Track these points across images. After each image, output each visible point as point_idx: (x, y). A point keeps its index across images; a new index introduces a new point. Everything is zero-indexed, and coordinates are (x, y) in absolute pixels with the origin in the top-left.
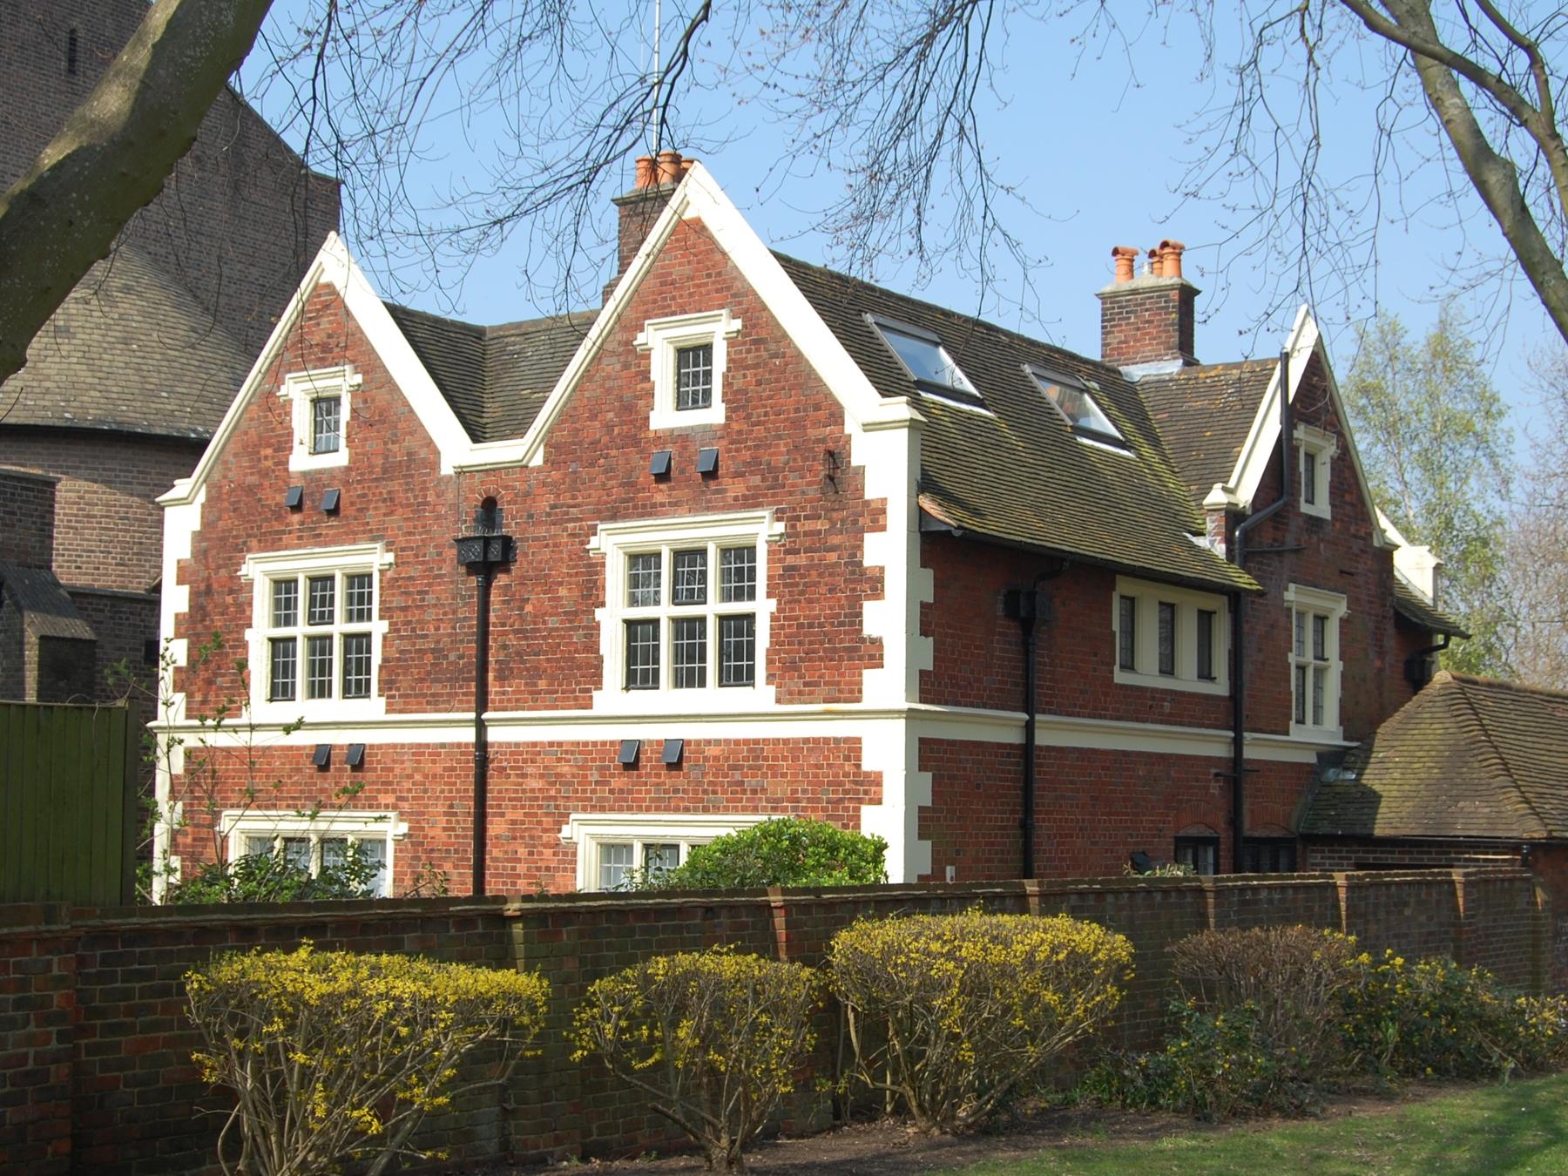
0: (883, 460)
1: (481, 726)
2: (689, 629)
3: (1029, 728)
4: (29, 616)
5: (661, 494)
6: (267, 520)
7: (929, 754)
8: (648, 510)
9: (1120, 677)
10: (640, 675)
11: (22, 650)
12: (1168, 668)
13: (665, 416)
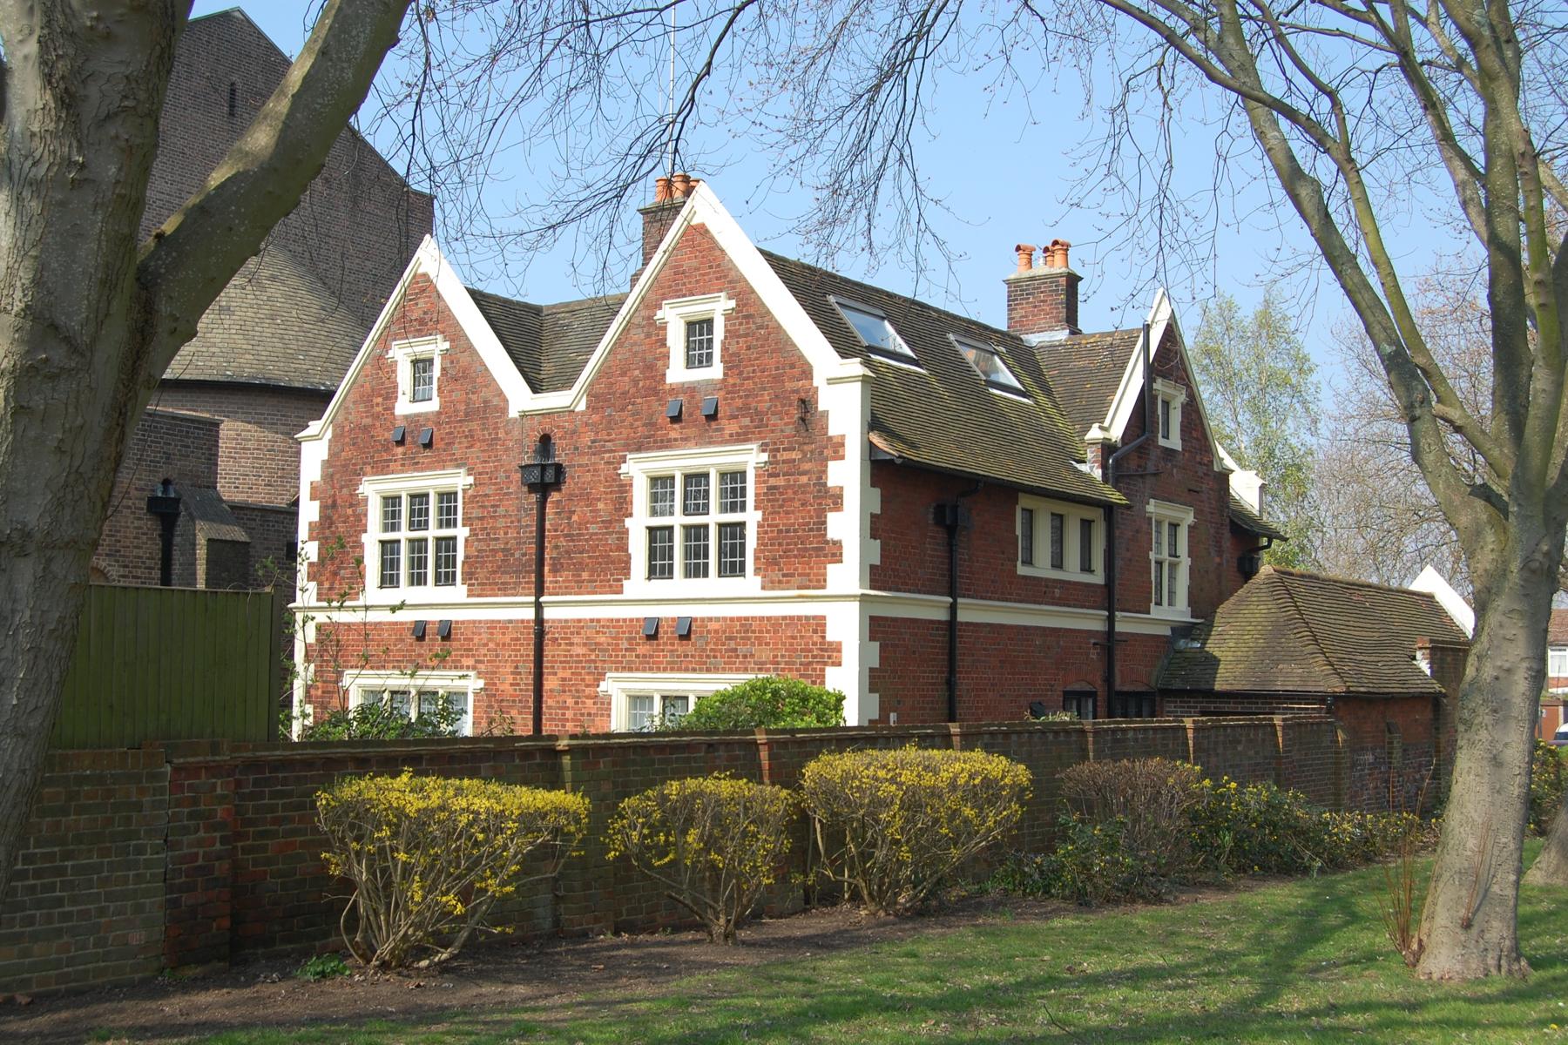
0: (842, 404)
1: (539, 607)
2: (696, 534)
3: (953, 609)
4: (199, 524)
5: (675, 432)
6: (378, 451)
7: (877, 628)
8: (665, 444)
9: (1022, 570)
10: (659, 568)
11: (194, 549)
12: (1058, 563)
13: (677, 373)
